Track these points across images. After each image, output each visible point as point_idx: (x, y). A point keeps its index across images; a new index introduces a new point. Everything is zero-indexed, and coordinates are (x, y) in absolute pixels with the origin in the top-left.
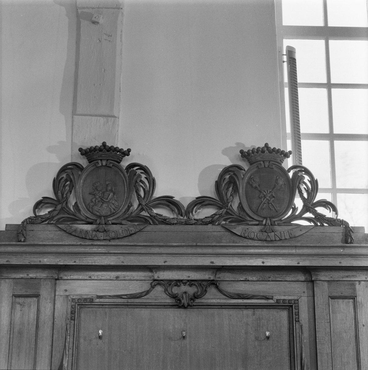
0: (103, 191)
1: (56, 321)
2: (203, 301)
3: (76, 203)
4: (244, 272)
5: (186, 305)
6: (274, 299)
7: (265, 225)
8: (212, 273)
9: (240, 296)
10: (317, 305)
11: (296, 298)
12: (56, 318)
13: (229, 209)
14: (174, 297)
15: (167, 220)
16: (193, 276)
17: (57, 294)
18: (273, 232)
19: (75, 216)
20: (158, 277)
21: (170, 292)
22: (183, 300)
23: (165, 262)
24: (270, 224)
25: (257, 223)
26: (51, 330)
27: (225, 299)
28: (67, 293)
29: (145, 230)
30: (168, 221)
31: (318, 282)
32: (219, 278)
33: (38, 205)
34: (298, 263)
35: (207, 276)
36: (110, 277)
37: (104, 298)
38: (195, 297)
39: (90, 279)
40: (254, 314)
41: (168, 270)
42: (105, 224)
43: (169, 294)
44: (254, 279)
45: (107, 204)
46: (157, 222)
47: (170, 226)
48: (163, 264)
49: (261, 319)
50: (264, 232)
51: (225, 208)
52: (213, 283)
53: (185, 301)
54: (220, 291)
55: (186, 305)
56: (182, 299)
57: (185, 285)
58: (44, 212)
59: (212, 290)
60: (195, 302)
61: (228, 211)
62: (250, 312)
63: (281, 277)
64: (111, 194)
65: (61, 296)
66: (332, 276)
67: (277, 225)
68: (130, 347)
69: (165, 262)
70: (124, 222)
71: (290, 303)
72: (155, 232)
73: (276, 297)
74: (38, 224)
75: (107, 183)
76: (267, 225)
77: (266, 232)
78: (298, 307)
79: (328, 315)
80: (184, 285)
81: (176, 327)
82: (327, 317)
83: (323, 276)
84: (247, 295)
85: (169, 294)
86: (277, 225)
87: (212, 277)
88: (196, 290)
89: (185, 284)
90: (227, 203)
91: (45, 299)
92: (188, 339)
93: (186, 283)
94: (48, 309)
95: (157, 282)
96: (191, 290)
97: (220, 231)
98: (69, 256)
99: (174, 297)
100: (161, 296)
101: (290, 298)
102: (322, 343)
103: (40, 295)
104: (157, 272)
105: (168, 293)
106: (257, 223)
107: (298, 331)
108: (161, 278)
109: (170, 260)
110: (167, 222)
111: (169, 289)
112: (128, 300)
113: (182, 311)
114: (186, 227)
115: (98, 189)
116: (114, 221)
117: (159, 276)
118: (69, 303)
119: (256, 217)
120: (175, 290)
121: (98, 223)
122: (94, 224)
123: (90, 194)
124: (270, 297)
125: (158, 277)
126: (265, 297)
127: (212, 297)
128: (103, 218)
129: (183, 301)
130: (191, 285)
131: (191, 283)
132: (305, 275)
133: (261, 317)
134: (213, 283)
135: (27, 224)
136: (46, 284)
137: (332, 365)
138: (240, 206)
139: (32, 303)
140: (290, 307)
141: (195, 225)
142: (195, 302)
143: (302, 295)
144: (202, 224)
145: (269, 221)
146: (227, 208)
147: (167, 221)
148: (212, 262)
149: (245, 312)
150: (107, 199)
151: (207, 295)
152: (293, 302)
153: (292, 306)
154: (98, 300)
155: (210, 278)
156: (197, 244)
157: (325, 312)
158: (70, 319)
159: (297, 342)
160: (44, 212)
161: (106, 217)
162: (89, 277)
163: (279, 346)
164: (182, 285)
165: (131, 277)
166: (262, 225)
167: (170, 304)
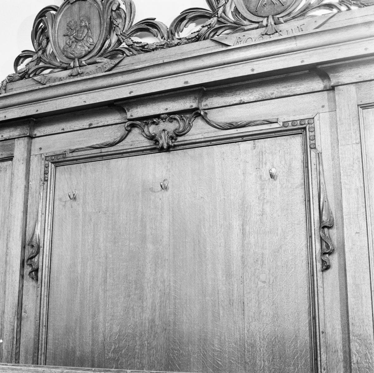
0: (77, 29)
1: (30, 184)
2: (190, 137)
3: (52, 51)
4: (238, 92)
5: (165, 146)
6: (279, 122)
7: (267, 26)
8: (194, 99)
9: (232, 126)
10: (340, 120)
11: (310, 116)
12: (30, 181)
13: (221, 17)
14: (152, 138)
15: (146, 47)
16: (171, 108)
17: (32, 154)
18: (277, 32)
19: (50, 64)
20: (131, 116)
21: (147, 133)
22: (161, 139)
23: (131, 93)
24: (273, 23)
25: (256, 25)
26: (23, 194)
27: (215, 131)
28: (42, 152)
29: (121, 65)
30: (147, 48)
31: (341, 87)
32: (206, 105)
33: (17, 63)
34: (302, 61)
35: (188, 104)
36: (84, 126)
37: (76, 152)
38: (178, 134)
39: (63, 131)
40: (255, 147)
41: (141, 104)
42: (80, 66)
43: (146, 135)
44: (252, 98)
45: (81, 43)
46: (135, 52)
47: (149, 53)
48: (129, 95)
49: (264, 153)
50: (265, 35)
51: (215, 16)
52: (195, 113)
53: (164, 141)
54: (208, 122)
55: (165, 146)
56: (160, 139)
57: (164, 121)
58: (22, 67)
59: (199, 123)
60: (177, 141)
61: (220, 19)
62: (247, 145)
63: (289, 90)
64: (86, 31)
65: (36, 155)
66: (360, 75)
67: (283, 22)
68: (105, 207)
69: (131, 93)
70: (98, 60)
71: (302, 125)
72: (133, 64)
73: (282, 119)
74: (17, 81)
75: (81, 18)
76: (269, 25)
77: (267, 34)
78: (314, 128)
79: (358, 132)
80: (164, 122)
81: (157, 176)
82: (356, 135)
83: (346, 76)
84: (242, 122)
85: (146, 135)
86: (283, 22)
87: (195, 104)
88: (177, 125)
89: (164, 119)
90: (217, 9)
91: (18, 160)
92: (170, 189)
93: (165, 119)
94: (21, 171)
95: (133, 124)
96: (171, 127)
97: (209, 46)
98: (32, 105)
99: (152, 138)
100: (139, 140)
101: (302, 117)
102: (349, 174)
103: (14, 157)
104: (129, 110)
105: (145, 135)
106: (256, 25)
107: (315, 162)
108: (135, 116)
109: (136, 89)
110: (145, 49)
111: (146, 130)
112: (101, 150)
113: (164, 155)
114: (168, 50)
115: (72, 28)
116: (89, 61)
117: (132, 115)
118: (43, 161)
119: (255, 19)
120: (152, 129)
121: (73, 67)
122: (69, 69)
123: (64, 36)
124: (275, 121)
125: (131, 116)
126: (267, 121)
127: (198, 131)
128: (76, 60)
129: (161, 142)
130: (172, 120)
131: (171, 116)
132: (323, 80)
133: (264, 150)
134: (195, 113)
135: (7, 83)
136: (20, 144)
137: (364, 205)
138: (236, 11)
139: (8, 167)
140: (300, 129)
141: (179, 45)
142: (177, 141)
143: (321, 111)
144: (187, 42)
145: (271, 19)
146: (217, 15)
147: (145, 48)
148: (186, 82)
149: (243, 145)
150: (81, 37)
151: (192, 131)
152: (307, 123)
153: (305, 128)
154: (70, 155)
155: (192, 106)
156: (163, 61)
157: (352, 129)
158: (43, 180)
159: (313, 177)
160: (22, 67)
161: (80, 58)
162: (62, 130)
163: (289, 187)
164: (161, 121)
165: (105, 122)
166: (263, 27)
167: (148, 148)
